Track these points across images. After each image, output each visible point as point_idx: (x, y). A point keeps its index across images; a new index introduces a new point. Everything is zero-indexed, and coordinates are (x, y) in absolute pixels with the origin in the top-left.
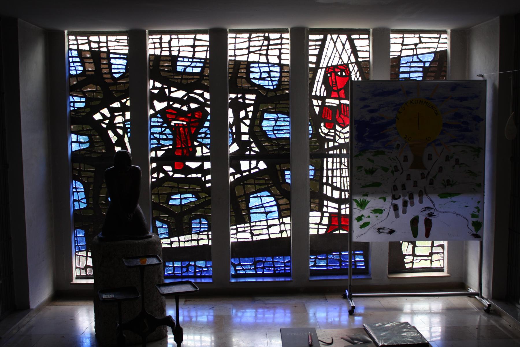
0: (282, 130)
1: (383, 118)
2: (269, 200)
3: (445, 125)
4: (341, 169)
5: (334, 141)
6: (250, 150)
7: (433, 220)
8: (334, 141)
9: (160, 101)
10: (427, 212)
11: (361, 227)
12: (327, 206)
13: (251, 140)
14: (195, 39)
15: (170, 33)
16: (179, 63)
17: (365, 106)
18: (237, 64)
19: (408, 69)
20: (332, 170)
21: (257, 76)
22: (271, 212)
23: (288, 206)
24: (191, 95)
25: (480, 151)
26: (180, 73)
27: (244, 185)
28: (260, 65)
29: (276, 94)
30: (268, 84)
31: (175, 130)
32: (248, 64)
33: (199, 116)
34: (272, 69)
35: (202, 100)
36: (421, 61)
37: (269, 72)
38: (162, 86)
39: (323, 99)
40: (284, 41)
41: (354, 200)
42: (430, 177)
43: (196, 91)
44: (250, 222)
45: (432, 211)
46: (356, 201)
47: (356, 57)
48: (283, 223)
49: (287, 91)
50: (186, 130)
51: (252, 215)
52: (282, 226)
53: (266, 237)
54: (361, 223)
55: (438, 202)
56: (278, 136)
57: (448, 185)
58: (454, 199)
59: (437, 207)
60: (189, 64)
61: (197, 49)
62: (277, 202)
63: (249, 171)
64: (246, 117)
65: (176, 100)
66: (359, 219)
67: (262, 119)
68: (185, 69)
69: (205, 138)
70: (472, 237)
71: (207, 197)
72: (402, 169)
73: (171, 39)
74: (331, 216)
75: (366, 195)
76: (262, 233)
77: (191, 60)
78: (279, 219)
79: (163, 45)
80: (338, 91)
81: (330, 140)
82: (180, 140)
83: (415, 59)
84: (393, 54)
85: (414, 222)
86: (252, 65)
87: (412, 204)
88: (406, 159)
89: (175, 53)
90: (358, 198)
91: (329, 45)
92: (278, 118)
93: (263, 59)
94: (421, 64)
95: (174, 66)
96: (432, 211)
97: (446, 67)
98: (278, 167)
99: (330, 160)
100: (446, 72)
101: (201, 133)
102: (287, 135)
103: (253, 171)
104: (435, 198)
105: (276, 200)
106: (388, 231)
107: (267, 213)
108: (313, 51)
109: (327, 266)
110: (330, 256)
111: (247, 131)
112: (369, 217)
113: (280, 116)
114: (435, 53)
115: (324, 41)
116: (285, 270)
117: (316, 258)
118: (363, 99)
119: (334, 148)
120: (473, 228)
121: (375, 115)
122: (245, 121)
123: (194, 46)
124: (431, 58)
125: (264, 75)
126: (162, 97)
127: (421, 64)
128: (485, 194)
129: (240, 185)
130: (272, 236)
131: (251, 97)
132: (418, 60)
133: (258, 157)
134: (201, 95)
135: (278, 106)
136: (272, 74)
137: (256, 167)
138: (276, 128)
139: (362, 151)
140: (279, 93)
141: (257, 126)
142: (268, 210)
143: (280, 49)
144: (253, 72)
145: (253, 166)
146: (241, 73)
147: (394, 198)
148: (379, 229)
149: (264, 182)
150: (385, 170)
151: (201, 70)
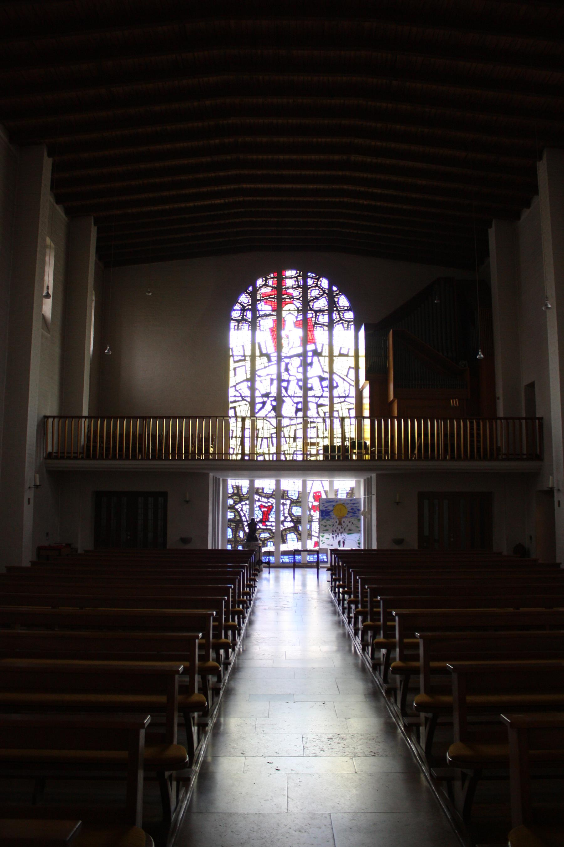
1: (329, 510)
3: (348, 512)
17: (324, 506)
31: (263, 512)
39: (312, 502)
42: (344, 528)
54: (323, 542)
58: (352, 535)
65: (263, 502)
66: (322, 541)
67: (292, 509)
69: (273, 515)
75: (324, 533)
85: (339, 542)
87: (338, 536)
88: (336, 522)
96: (345, 539)
98: (297, 525)
106: (331, 545)
118: (323, 504)
120: (358, 544)
121: (327, 508)
124: (349, 489)
133: (290, 521)
138: (297, 512)
139: (323, 519)
140: (298, 500)
142: (293, 540)
145: (289, 525)
148: (328, 544)
150: (330, 525)
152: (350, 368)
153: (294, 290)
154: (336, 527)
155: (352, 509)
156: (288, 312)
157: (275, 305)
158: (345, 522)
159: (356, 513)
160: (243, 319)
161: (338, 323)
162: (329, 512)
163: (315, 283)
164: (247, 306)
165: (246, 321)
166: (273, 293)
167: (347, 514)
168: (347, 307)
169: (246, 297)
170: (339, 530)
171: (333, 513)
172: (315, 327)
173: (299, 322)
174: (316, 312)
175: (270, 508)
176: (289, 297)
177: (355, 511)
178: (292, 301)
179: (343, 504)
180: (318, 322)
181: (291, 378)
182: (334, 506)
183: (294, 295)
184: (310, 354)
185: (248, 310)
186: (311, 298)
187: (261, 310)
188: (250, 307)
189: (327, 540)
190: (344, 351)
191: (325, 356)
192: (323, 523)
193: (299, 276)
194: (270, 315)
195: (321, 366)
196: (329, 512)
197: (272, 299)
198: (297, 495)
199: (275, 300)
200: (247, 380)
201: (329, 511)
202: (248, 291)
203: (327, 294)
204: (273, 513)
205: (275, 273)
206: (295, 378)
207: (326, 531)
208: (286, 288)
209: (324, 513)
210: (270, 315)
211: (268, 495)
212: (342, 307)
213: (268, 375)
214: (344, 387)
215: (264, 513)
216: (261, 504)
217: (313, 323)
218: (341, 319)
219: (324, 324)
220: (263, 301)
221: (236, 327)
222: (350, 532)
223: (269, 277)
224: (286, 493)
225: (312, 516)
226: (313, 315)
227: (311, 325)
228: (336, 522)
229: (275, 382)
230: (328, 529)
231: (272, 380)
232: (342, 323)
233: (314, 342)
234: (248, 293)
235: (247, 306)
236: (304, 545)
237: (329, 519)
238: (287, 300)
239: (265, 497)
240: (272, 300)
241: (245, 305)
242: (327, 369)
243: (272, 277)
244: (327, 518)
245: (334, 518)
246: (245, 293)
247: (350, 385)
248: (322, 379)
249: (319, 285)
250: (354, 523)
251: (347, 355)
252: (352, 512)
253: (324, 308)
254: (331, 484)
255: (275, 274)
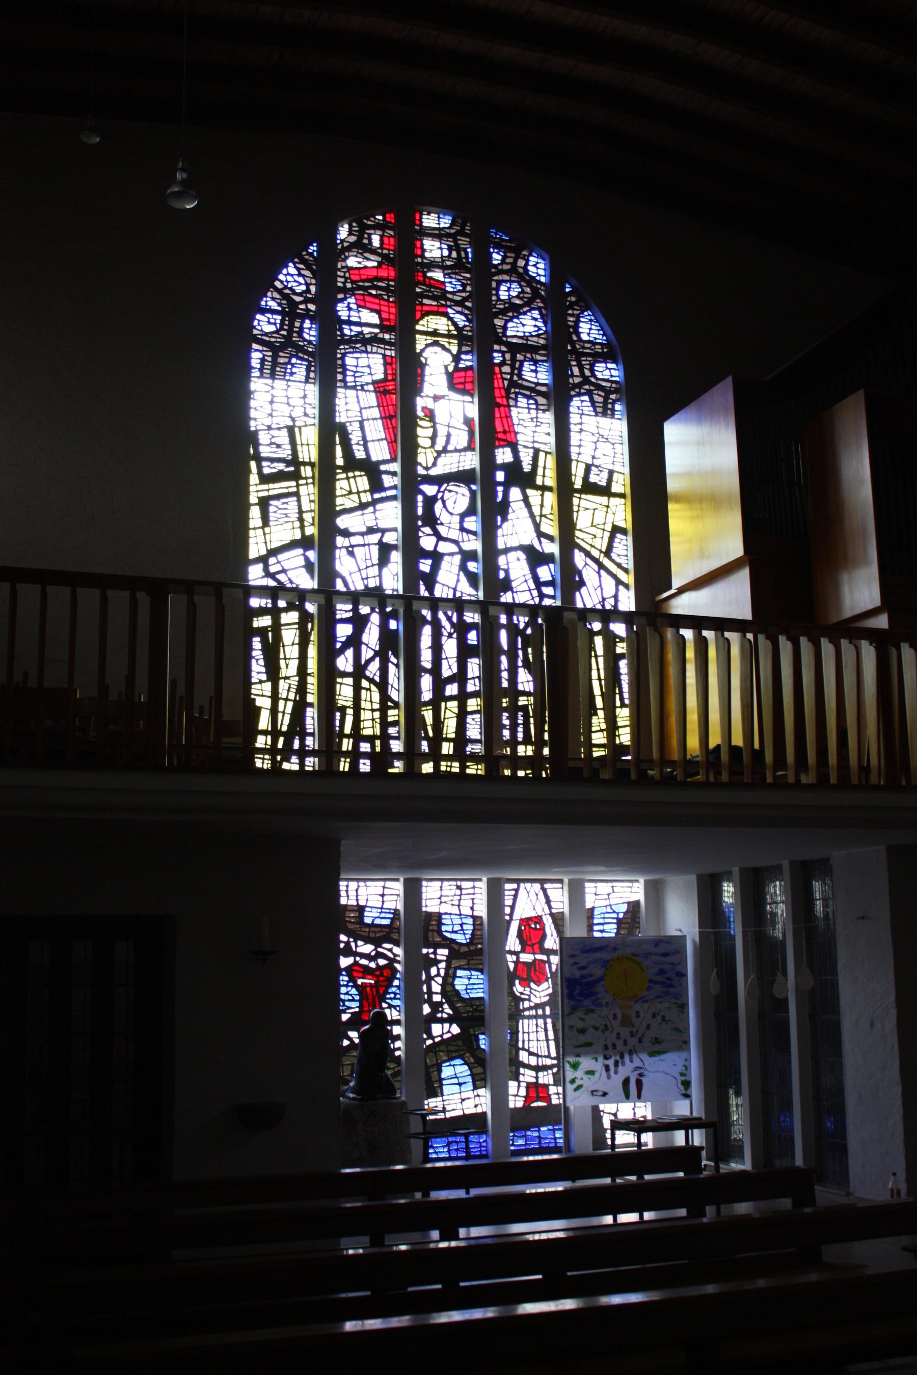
0: (476, 989)
1: (592, 976)
2: (462, 1070)
3: (651, 981)
4: (537, 1032)
5: (529, 1000)
6: (442, 1012)
7: (644, 1080)
8: (529, 1000)
9: (346, 956)
10: (637, 1072)
11: (576, 1090)
12: (523, 1075)
13: (444, 1001)
14: (384, 887)
15: (358, 880)
16: (366, 914)
17: (575, 964)
18: (429, 915)
19: (602, 921)
20: (528, 1033)
21: (449, 928)
22: (465, 1083)
23: (483, 1076)
24: (380, 950)
25: (684, 1007)
26: (367, 925)
27: (436, 1053)
28: (453, 917)
29: (469, 949)
30: (460, 938)
31: (361, 989)
32: (439, 916)
33: (388, 973)
34: (464, 921)
35: (392, 956)
36: (614, 912)
37: (461, 925)
38: (348, 940)
39: (516, 954)
40: (477, 890)
41: (567, 1061)
42: (639, 1035)
43: (385, 945)
44: (442, 1095)
45: (642, 1071)
46: (569, 1062)
47: (550, 908)
48: (478, 1096)
49: (480, 946)
50: (374, 990)
51: (444, 1087)
52: (477, 1098)
53: (460, 1113)
54: (575, 1085)
55: (649, 1062)
56: (472, 996)
57: (656, 1043)
58: (663, 1057)
59: (647, 1066)
60: (378, 915)
61: (386, 898)
62: (471, 1071)
63: (441, 1036)
64: (438, 975)
65: (363, 956)
66: (573, 1081)
67: (455, 976)
68: (373, 920)
69: (395, 998)
70: (683, 1097)
71: (396, 1067)
72: (612, 1027)
73: (359, 886)
74: (529, 1086)
75: (578, 1056)
76: (455, 1108)
77: (379, 910)
78: (473, 1090)
79: (350, 893)
80: (532, 945)
81: (525, 999)
82: (367, 1001)
83: (609, 910)
84: (588, 905)
85: (626, 1082)
86: (444, 917)
87: (623, 1064)
88: (615, 1017)
89: (362, 903)
90: (572, 1059)
91: (522, 892)
92: (472, 975)
93: (455, 910)
94: (615, 915)
95: (362, 916)
96: (642, 1071)
97: (639, 918)
98: (471, 1031)
99: (526, 1021)
100: (639, 923)
101: (389, 993)
102: (481, 995)
103: (445, 1037)
104: (644, 1056)
105: (470, 1069)
106: (601, 1093)
107: (460, 1084)
108: (508, 901)
109: (526, 1144)
110: (529, 1133)
111: (439, 991)
112: (582, 1079)
113: (474, 973)
114: (629, 903)
115: (517, 890)
116: (480, 1151)
117: (514, 1136)
118: (572, 956)
119: (530, 1008)
120: (682, 1088)
121: (585, 972)
122: (435, 979)
123: (383, 895)
124: (624, 908)
125: (457, 928)
126: (348, 952)
127: (615, 915)
128: (692, 1051)
129: (432, 1052)
130: (467, 1112)
131: (443, 953)
132: (611, 911)
133: (450, 1020)
134: (390, 950)
135: (472, 962)
136: (465, 927)
137: (449, 1032)
138: (469, 987)
139: (574, 1009)
140: (472, 948)
141: (449, 984)
142: (461, 1080)
143: (473, 899)
144: (444, 924)
145: (446, 1030)
146: (433, 925)
147: (606, 1058)
148: (592, 1092)
149: (456, 1048)
150: (596, 1028)
151: (391, 922)
152: (616, 530)
153: (448, 274)
154: (615, 1032)
155: (662, 972)
156: (430, 340)
157: (389, 313)
158: (642, 1014)
159: (671, 986)
160: (288, 343)
161: (577, 390)
162: (593, 984)
163: (508, 260)
164: (301, 303)
165: (301, 349)
166: (383, 273)
167: (648, 989)
168: (600, 347)
169: (300, 275)
170: (625, 1043)
171: (604, 986)
172: (513, 396)
173: (462, 374)
174: (514, 349)
175: (385, 975)
176: (432, 292)
177: (669, 979)
178: (442, 305)
179: (634, 955)
180: (520, 382)
181: (443, 547)
182: (605, 964)
183: (449, 288)
184: (500, 476)
185: (307, 315)
186: (497, 306)
187: (349, 323)
188: (312, 307)
189: (590, 1076)
190: (598, 478)
191: (544, 488)
192: (573, 1020)
193: (461, 233)
194: (375, 340)
195: (532, 516)
196: (593, 984)
197: (379, 292)
198: (469, 928)
199: (389, 297)
200: (305, 543)
201: (590, 979)
202: (307, 257)
203: (543, 300)
204: (395, 994)
205: (390, 212)
206: (454, 548)
207: (584, 1049)
208: (423, 265)
209: (578, 987)
210: (375, 340)
211: (377, 930)
212: (587, 345)
213: (371, 531)
214: (600, 586)
215: (367, 995)
216: (356, 963)
217: (506, 383)
218: (586, 381)
219: (539, 388)
220: (354, 295)
221: (268, 365)
222: (657, 1048)
223: (369, 223)
224: (434, 923)
225: (517, 1000)
226: (503, 356)
227: (500, 388)
228: (615, 1017)
229: (396, 557)
230: (590, 1040)
231: (385, 550)
232: (589, 393)
233: (509, 439)
234: (303, 261)
235: (301, 303)
236: (499, 1098)
237: (592, 1007)
238: (426, 301)
239: (367, 941)
240: (381, 295)
241: (298, 299)
242: (550, 527)
243: (378, 223)
244: (587, 1002)
245: (607, 1003)
246: (296, 260)
247: (619, 582)
248: (535, 558)
249: (521, 270)
250: (667, 1018)
251: (605, 491)
252: (662, 983)
253: (535, 339)
254: (576, 893)
255: (388, 216)
